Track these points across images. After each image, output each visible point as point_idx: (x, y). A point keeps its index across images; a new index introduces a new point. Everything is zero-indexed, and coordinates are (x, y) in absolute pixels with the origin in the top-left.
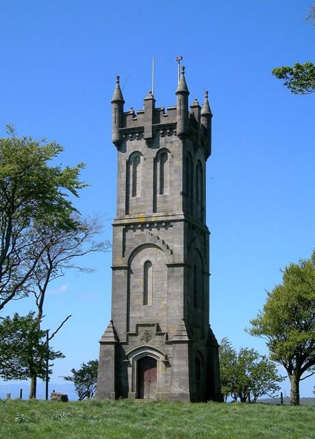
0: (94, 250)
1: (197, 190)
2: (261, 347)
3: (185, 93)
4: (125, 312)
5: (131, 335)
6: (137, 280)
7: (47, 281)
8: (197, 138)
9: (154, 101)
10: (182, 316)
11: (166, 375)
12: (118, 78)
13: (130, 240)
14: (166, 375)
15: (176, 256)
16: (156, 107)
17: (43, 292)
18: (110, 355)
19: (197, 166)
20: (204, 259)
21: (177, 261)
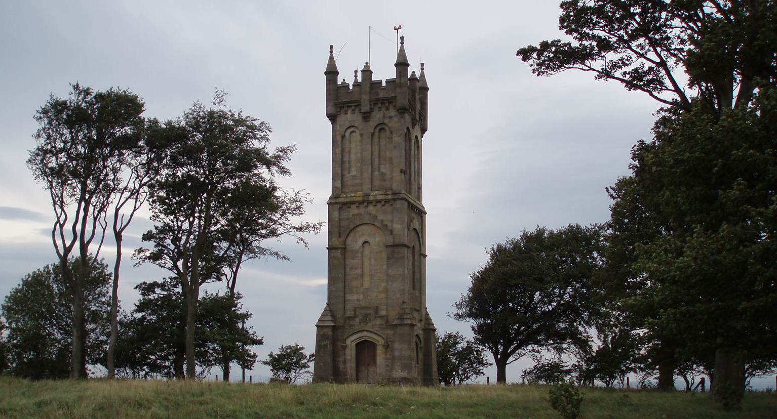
1: (415, 167)
2: (466, 330)
5: (349, 318)
8: (415, 113)
12: (331, 47)
14: (387, 359)
17: (235, 273)
19: (415, 142)
20: (421, 240)
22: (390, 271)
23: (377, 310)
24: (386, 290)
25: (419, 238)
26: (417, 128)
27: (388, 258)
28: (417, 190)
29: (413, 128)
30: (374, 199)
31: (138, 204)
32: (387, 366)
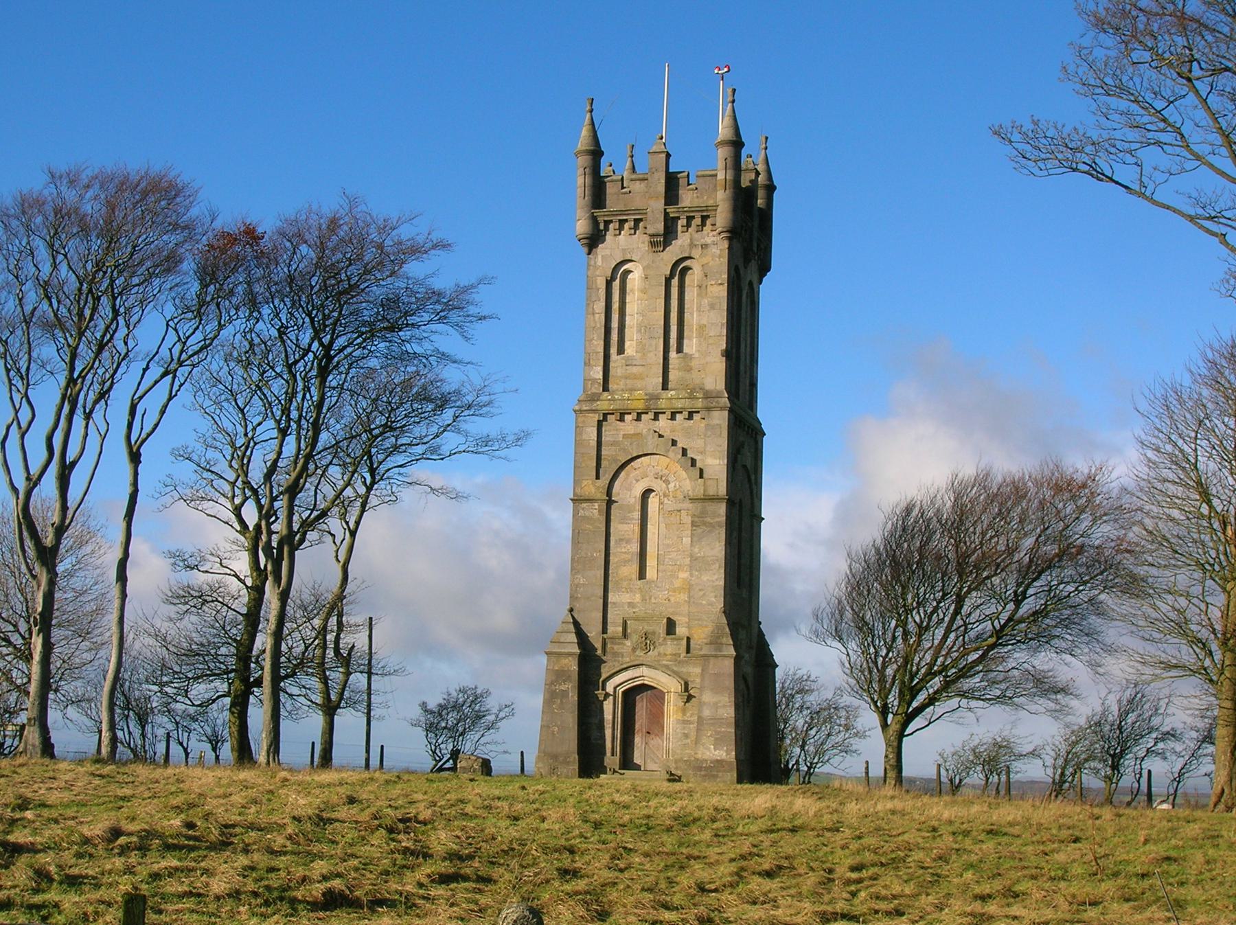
0: (468, 452)
3: (737, 144)
4: (600, 592)
6: (624, 528)
7: (363, 510)
9: (668, 156)
10: (720, 604)
11: (685, 722)
13: (614, 444)
14: (685, 722)
15: (709, 482)
16: (670, 171)
17: (353, 534)
18: (569, 678)
20: (754, 487)
21: (711, 492)
22: (696, 550)
23: (671, 626)
24: (689, 587)
25: (750, 480)
26: (753, 266)
27: (693, 524)
28: (748, 388)
29: (746, 268)
30: (669, 406)
31: (176, 387)
32: (686, 736)
